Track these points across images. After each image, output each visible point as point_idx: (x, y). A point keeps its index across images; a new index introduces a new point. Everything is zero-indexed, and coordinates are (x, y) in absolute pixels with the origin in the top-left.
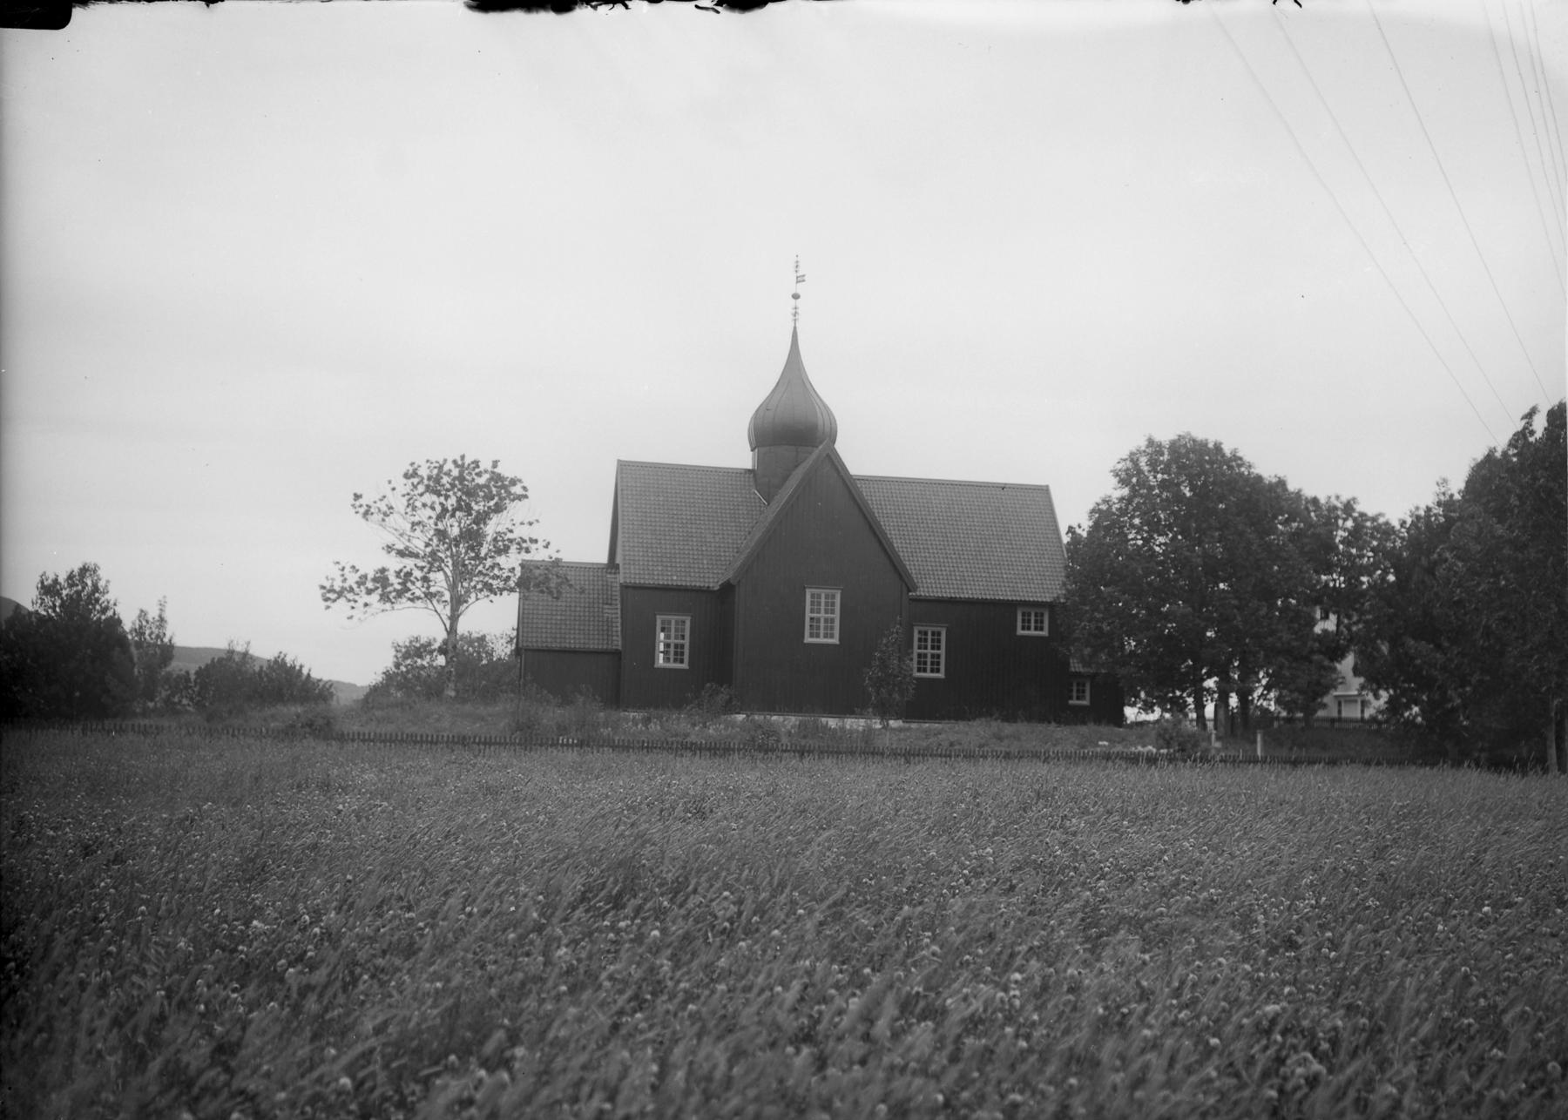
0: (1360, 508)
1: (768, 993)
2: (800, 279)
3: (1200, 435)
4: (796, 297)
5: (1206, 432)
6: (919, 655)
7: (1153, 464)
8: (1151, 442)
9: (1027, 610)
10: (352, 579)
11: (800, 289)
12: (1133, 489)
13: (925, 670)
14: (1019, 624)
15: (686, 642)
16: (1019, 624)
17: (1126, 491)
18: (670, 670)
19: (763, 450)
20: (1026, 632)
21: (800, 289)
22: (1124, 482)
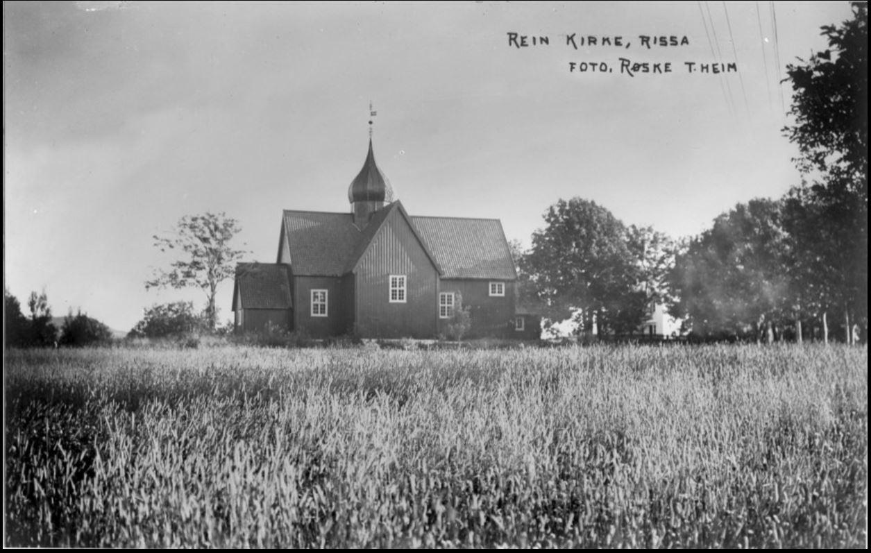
0: (655, 229)
1: (101, 483)
2: (373, 114)
3: (584, 198)
4: (371, 123)
5: (587, 197)
6: (314, 305)
7: (561, 211)
8: (560, 201)
9: (494, 283)
10: (159, 275)
11: (373, 119)
12: (552, 224)
13: (317, 313)
14: (490, 291)
15: (326, 303)
16: (490, 291)
17: (549, 225)
18: (319, 318)
19: (359, 203)
20: (450, 294)
21: (373, 119)
22: (548, 221)
